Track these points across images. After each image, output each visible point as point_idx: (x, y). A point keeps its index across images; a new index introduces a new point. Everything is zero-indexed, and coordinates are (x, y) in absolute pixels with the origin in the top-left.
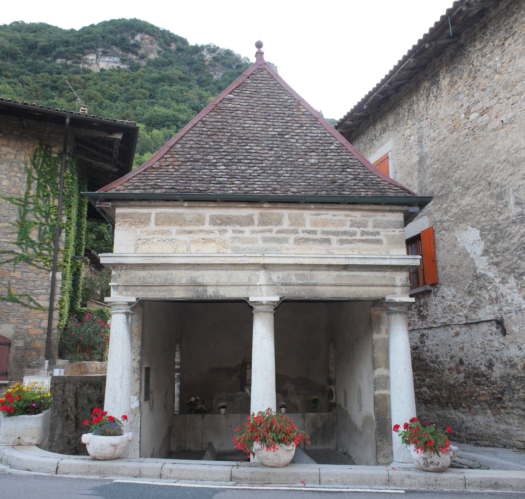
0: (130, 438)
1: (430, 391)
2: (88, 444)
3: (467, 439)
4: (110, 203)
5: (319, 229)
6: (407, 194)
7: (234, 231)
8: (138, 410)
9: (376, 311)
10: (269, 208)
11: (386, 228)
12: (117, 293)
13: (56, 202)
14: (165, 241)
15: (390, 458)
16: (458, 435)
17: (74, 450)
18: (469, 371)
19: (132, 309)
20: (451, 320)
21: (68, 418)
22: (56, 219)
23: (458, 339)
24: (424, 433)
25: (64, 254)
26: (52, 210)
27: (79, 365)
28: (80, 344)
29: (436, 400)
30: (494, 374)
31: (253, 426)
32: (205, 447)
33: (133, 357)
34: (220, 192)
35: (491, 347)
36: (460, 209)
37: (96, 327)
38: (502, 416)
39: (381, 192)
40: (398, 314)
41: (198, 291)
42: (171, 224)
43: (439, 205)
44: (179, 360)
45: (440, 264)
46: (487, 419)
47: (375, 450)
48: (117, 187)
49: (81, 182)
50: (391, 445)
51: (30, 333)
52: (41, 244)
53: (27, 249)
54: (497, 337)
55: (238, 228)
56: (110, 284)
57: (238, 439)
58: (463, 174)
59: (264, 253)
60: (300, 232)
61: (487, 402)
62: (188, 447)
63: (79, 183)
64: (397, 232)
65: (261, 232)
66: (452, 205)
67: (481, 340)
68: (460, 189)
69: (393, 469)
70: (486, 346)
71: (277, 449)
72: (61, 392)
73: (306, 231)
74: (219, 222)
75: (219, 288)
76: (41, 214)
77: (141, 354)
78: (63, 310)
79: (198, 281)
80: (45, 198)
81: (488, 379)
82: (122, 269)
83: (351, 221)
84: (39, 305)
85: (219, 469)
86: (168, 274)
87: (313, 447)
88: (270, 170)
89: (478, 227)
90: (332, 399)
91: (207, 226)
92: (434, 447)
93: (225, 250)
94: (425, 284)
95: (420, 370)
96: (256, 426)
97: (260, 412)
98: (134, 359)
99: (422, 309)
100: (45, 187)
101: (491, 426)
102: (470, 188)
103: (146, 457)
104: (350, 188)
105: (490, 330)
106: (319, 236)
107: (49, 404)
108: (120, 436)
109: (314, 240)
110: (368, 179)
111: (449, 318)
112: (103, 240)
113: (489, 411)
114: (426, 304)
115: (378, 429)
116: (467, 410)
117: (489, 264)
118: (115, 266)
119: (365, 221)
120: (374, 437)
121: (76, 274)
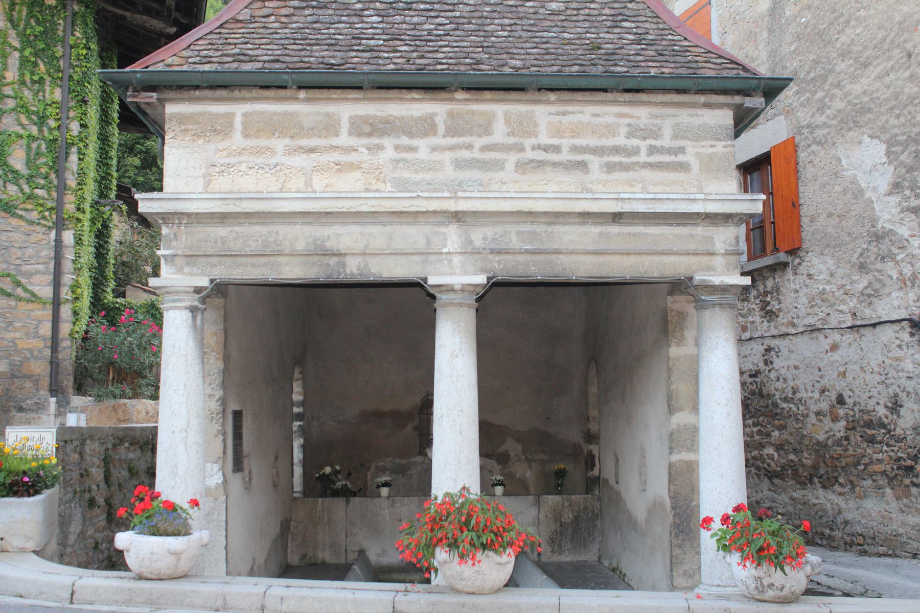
0: (206, 540)
1: (779, 455)
2: (128, 551)
3: (846, 543)
4: (154, 94)
5: (566, 143)
6: (741, 72)
7: (397, 148)
8: (222, 490)
9: (677, 303)
10: (466, 100)
11: (697, 140)
12: (173, 270)
13: (58, 95)
14: (263, 168)
15: (697, 577)
16: (823, 535)
17: (106, 562)
18: (854, 416)
19: (203, 300)
20: (825, 321)
21: (92, 503)
22: (59, 127)
23: (836, 356)
24: (758, 532)
25: (76, 195)
26: (50, 109)
27: (114, 407)
28: (114, 367)
29: (790, 472)
30: (902, 423)
31: (435, 519)
32: (352, 557)
33: (209, 391)
34: (370, 67)
35: (897, 372)
36: (849, 102)
37: (143, 335)
38: (913, 499)
39: (690, 68)
40: (717, 309)
41: (328, 265)
42: (274, 134)
43: (808, 95)
44: (301, 398)
45: (806, 212)
46: (885, 505)
47: (668, 562)
48: (168, 59)
49: (105, 54)
50: (698, 553)
51: (20, 347)
52: (32, 177)
53: (5, 187)
54: (911, 351)
55: (405, 141)
56: (159, 253)
57: (405, 543)
58: (858, 35)
59: (455, 189)
60: (528, 149)
61: (887, 475)
63: (101, 57)
64: (720, 147)
65: (451, 148)
66: (833, 95)
67: (880, 358)
68: (851, 66)
69: (699, 597)
70: (888, 369)
71: (479, 562)
72: (77, 456)
73: (539, 147)
74: (367, 129)
75: (370, 260)
76: (28, 118)
77: (224, 385)
78: (78, 304)
79: (328, 245)
80: (36, 86)
81: (889, 432)
82: (180, 223)
83: (629, 125)
84: (34, 295)
85: (372, 598)
86: (270, 233)
87: (556, 558)
88: (470, 23)
89: (883, 137)
90: (592, 470)
91: (344, 139)
92: (777, 558)
93: (381, 186)
94: (776, 250)
95: (762, 415)
96: (441, 519)
97: (447, 494)
98: (210, 396)
99: (768, 299)
100: (35, 64)
101: (890, 518)
102: (869, 64)
103: (239, 575)
104: (628, 61)
105: (897, 338)
106: (565, 156)
107: (55, 477)
108: (187, 537)
109: (555, 165)
110: (664, 43)
111: (821, 315)
112: (154, 169)
113: (888, 490)
114: (777, 289)
115: (675, 525)
116: (847, 490)
117: (902, 211)
118: (167, 217)
119: (656, 125)
120: (666, 539)
121: (102, 235)
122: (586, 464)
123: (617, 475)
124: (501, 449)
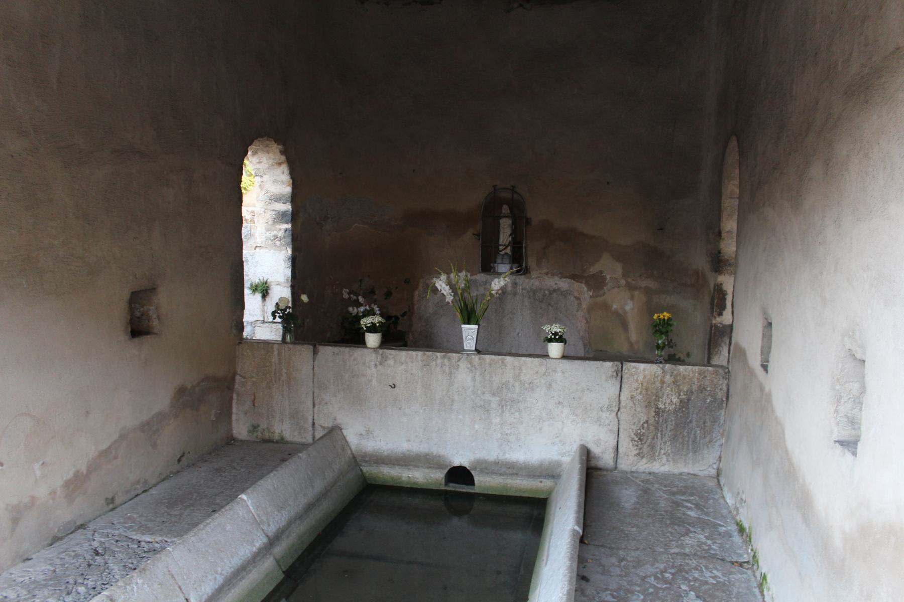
62: (277, 431)
87: (643, 466)
90: (720, 314)
122: (712, 303)
123: (766, 351)
124: (594, 269)
